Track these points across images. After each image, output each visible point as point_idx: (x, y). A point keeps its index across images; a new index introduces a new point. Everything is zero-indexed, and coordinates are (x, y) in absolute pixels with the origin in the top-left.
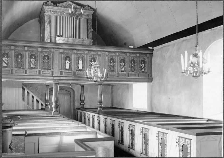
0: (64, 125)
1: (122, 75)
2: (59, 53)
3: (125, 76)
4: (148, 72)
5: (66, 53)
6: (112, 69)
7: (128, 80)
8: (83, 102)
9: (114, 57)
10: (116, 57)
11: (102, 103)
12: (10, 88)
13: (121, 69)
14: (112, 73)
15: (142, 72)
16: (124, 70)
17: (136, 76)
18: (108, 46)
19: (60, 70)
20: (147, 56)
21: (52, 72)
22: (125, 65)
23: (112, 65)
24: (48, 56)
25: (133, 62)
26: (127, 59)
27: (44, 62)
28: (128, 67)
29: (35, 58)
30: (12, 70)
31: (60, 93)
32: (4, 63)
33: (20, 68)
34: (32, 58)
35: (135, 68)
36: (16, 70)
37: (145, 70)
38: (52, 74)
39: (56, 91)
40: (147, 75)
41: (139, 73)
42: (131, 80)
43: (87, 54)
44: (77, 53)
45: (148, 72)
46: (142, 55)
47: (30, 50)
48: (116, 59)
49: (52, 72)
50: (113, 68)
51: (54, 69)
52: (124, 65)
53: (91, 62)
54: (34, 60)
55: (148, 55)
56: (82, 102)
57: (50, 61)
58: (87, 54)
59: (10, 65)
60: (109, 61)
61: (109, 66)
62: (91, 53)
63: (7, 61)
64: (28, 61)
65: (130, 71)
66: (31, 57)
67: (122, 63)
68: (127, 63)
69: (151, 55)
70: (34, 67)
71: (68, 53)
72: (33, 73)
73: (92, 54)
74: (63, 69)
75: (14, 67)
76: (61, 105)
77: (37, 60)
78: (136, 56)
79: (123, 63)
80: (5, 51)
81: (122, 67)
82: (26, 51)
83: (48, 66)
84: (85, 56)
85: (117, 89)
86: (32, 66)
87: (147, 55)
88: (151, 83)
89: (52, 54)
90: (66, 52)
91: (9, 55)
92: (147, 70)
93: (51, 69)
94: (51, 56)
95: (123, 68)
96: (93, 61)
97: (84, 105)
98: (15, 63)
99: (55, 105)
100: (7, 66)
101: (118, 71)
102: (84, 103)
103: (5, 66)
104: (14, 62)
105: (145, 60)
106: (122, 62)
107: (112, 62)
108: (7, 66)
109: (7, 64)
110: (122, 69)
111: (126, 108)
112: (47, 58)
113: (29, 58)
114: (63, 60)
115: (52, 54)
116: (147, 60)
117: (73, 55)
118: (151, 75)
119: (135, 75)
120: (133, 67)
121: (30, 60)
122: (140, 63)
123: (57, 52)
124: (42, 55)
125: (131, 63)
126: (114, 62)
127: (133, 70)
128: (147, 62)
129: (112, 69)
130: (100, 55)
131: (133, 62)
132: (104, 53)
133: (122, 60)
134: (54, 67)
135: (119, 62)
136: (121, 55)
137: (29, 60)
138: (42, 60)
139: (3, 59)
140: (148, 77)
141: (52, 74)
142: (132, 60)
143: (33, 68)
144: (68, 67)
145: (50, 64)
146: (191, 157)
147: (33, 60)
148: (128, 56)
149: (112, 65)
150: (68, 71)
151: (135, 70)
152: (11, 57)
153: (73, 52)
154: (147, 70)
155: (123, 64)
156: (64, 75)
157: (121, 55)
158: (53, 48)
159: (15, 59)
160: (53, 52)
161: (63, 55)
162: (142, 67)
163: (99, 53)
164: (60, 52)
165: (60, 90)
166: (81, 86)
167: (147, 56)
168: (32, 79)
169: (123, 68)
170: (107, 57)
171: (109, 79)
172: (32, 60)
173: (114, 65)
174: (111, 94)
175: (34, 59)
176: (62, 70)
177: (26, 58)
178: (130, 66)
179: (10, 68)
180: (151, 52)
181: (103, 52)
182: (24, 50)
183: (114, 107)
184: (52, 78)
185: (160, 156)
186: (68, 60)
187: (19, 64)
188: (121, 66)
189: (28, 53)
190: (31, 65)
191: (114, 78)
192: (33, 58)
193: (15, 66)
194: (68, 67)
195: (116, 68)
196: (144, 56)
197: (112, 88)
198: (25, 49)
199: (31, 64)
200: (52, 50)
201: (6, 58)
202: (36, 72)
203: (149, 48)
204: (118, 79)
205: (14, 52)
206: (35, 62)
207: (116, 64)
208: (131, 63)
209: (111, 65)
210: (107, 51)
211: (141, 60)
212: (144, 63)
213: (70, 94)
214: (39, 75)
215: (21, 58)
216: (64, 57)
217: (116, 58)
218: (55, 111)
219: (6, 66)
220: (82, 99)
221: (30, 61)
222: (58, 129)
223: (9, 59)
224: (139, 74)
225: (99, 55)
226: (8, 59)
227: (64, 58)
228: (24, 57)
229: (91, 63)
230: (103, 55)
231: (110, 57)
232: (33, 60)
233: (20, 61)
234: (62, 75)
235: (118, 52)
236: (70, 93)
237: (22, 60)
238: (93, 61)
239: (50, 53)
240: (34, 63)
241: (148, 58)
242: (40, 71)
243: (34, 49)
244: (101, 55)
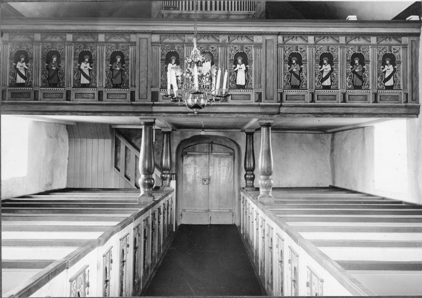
0: (23, 213)
1: (325, 98)
2: (150, 44)
3: (44, 94)
4: (405, 88)
5: (166, 43)
6: (295, 81)
7: (342, 110)
8: (251, 173)
9: (301, 49)
10: (308, 49)
11: (270, 174)
12: (106, 140)
13: (322, 81)
14: (357, 92)
15: (388, 88)
16: (330, 84)
17: (366, 99)
18: (275, 19)
19: (153, 90)
20: (403, 43)
21: (133, 93)
22: (332, 69)
23: (294, 72)
24: (89, 54)
25: (357, 62)
26: (339, 53)
27: (112, 69)
28: (342, 75)
29: (90, 62)
30: (36, 92)
31: (210, 151)
32: (18, 76)
33: (55, 85)
34: (84, 61)
35: (365, 77)
36: (45, 92)
37: (394, 82)
38: (133, 99)
39: (147, 144)
40: (403, 98)
41: (376, 91)
42: (351, 110)
43: (223, 45)
44: (109, 41)
45: (405, 88)
46: (388, 40)
47: (80, 40)
48: (308, 55)
49: (133, 93)
50: (298, 77)
51: (137, 88)
52: (330, 69)
53: (234, 66)
54: (88, 64)
55: (405, 40)
56: (248, 172)
57: (128, 65)
58: (223, 45)
59: (32, 79)
60: (285, 61)
61: (285, 74)
62: (236, 41)
63: (25, 69)
64: (72, 70)
65: (350, 86)
66: (81, 60)
67: (325, 64)
68: (339, 65)
69: (415, 39)
70: (22, 81)
71: (173, 44)
72: (85, 97)
73: (238, 44)
74: (160, 86)
75: (40, 85)
76: (212, 179)
77: (96, 66)
78: (251, 42)
79: (390, 64)
80: (85, 47)
81: (386, 76)
82: (102, 44)
83: (122, 80)
84: (220, 48)
85: (343, 141)
86: (84, 81)
87: (372, 38)
88: (416, 120)
89: (131, 49)
90: (167, 40)
91: (215, 58)
92: (401, 83)
93: (130, 86)
94: (130, 53)
95: (329, 79)
96: (240, 61)
97: (253, 179)
98: (42, 74)
99: (145, 180)
100: (24, 82)
101: (311, 87)
102: (254, 175)
103: (21, 83)
104: (40, 72)
105: (396, 55)
106: (325, 62)
107: (294, 62)
108: (24, 82)
109: (90, 79)
110: (326, 81)
111: (359, 190)
112: (119, 60)
113: (76, 62)
114: (160, 61)
115: (131, 49)
116: (400, 54)
117: (185, 48)
118: (414, 96)
119: (365, 98)
120: (296, 75)
121: (79, 67)
122: (379, 62)
123: (145, 41)
124: (106, 53)
125: (353, 63)
126: (300, 62)
127: (359, 82)
128: (402, 60)
129: (295, 81)
130: (261, 44)
131: (357, 62)
132: (272, 40)
133: (324, 55)
134: (137, 81)
135: (317, 61)
136: (320, 42)
137: (75, 65)
138: (107, 66)
139: (18, 67)
140: (407, 102)
141: (133, 99)
142: (355, 56)
143: (84, 86)
144: (241, 79)
145: (126, 73)
146: (3, 249)
147: (85, 66)
148: (342, 44)
149: (294, 70)
150: (242, 92)
151: (363, 82)
152: (34, 61)
153: (186, 41)
154: (401, 83)
155: (327, 68)
156: (106, 100)
157: (320, 42)
158: (135, 33)
159: (43, 64)
160: (135, 43)
161: (160, 49)
162: (387, 75)
163: (258, 39)
164: (153, 41)
165: (210, 145)
166: (247, 134)
167: (403, 43)
168: (54, 111)
169: (329, 79)
170: (281, 51)
171: (285, 108)
172: (83, 65)
173: (301, 71)
174: (331, 155)
175: (87, 62)
176: (157, 89)
177: (69, 62)
178: (347, 74)
179: (30, 86)
180: (415, 31)
181: (268, 37)
182: (64, 42)
183: (336, 185)
184: (131, 109)
185: (293, 295)
186: (174, 61)
187: (118, 75)
188: (322, 72)
189: (105, 49)
190: (80, 79)
191: (299, 106)
192: (87, 60)
193: (43, 81)
194: (241, 79)
195: (307, 79)
196: (393, 42)
197: (333, 139)
198: (67, 40)
199: (82, 75)
200: (133, 38)
201: (24, 64)
202: (92, 95)
203: (407, 19)
204: (313, 110)
205: (41, 47)
206: (90, 70)
207: (306, 67)
208: (353, 63)
209: (292, 72)
210: (279, 34)
211: (382, 54)
212: (393, 63)
213: (233, 154)
214: (68, 102)
215: (58, 61)
216: (162, 55)
217: (308, 52)
218: (143, 195)
219: (22, 82)
220: (247, 166)
221: (77, 67)
222: (146, 234)
223: (29, 64)
224: (376, 95)
225: (258, 46)
226: (27, 66)
227: (164, 57)
228: (64, 59)
229: (235, 68)
230: (269, 44)
231: (289, 49)
232: (85, 66)
233: (54, 68)
234: (157, 101)
235: (311, 34)
236: (231, 151)
237: (60, 66)
238: (359, 62)
239: (128, 46)
240: (88, 74)
241: (405, 46)
242: (70, 91)
243: (88, 38)
244: (264, 46)
